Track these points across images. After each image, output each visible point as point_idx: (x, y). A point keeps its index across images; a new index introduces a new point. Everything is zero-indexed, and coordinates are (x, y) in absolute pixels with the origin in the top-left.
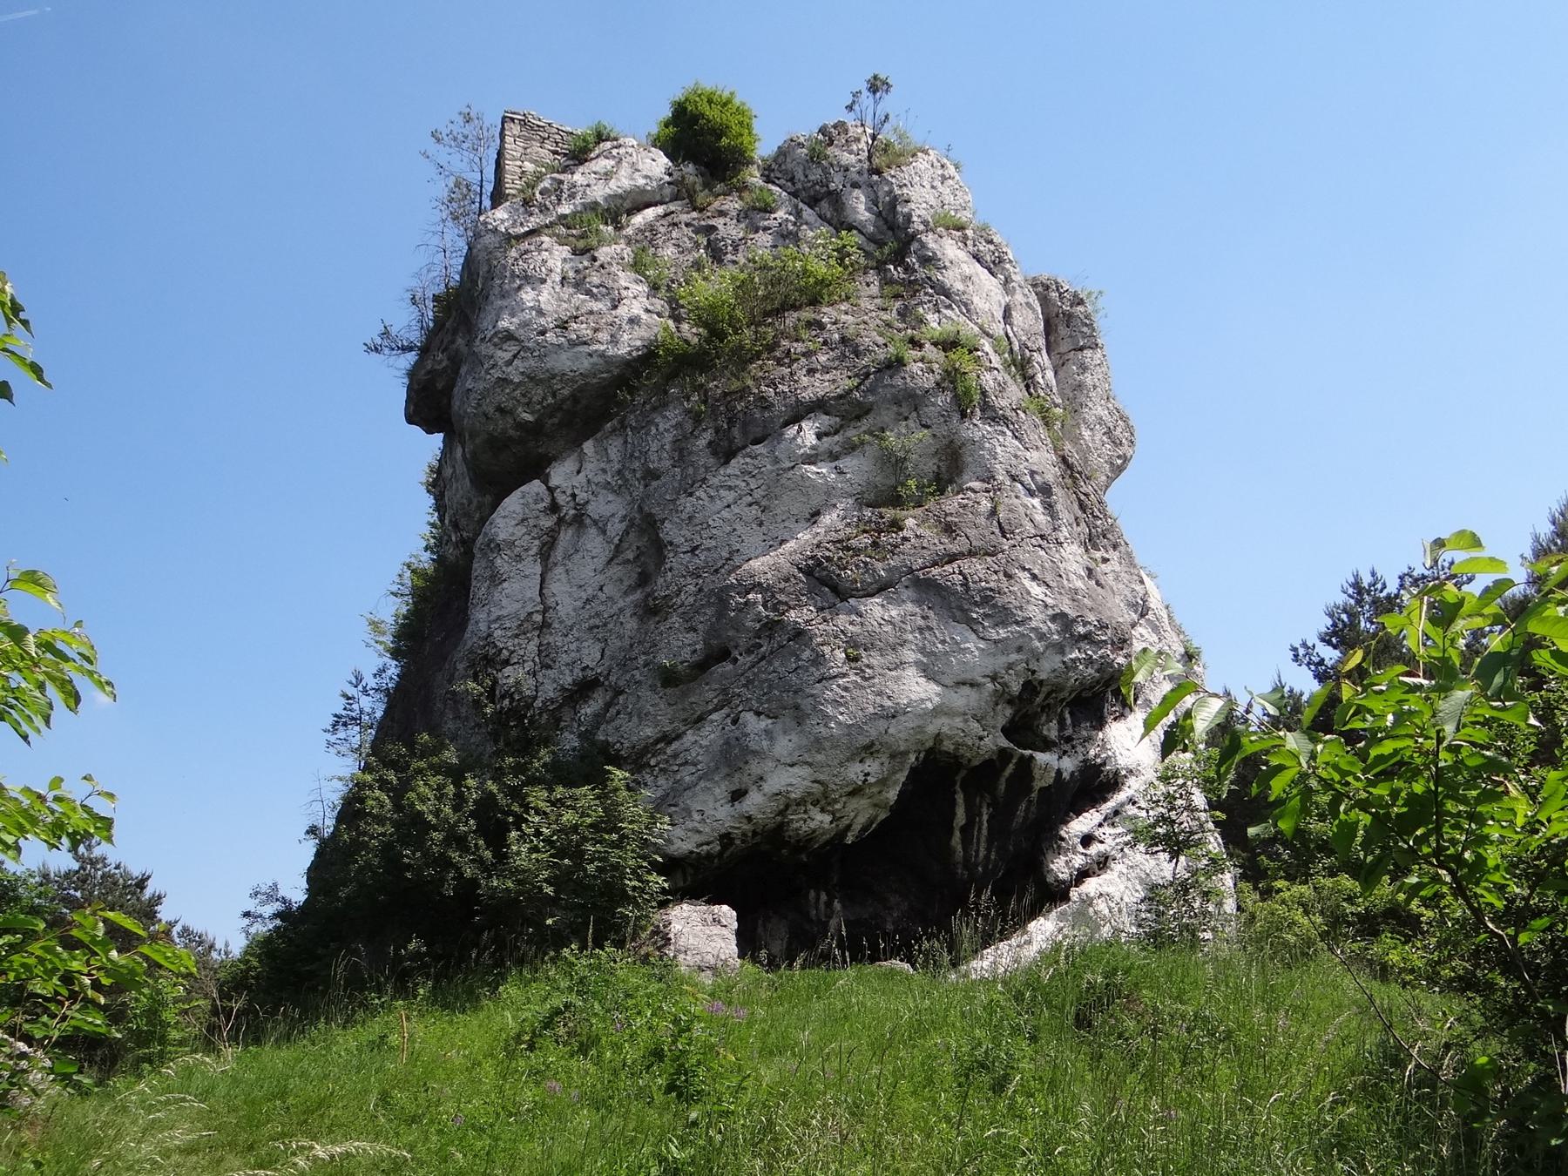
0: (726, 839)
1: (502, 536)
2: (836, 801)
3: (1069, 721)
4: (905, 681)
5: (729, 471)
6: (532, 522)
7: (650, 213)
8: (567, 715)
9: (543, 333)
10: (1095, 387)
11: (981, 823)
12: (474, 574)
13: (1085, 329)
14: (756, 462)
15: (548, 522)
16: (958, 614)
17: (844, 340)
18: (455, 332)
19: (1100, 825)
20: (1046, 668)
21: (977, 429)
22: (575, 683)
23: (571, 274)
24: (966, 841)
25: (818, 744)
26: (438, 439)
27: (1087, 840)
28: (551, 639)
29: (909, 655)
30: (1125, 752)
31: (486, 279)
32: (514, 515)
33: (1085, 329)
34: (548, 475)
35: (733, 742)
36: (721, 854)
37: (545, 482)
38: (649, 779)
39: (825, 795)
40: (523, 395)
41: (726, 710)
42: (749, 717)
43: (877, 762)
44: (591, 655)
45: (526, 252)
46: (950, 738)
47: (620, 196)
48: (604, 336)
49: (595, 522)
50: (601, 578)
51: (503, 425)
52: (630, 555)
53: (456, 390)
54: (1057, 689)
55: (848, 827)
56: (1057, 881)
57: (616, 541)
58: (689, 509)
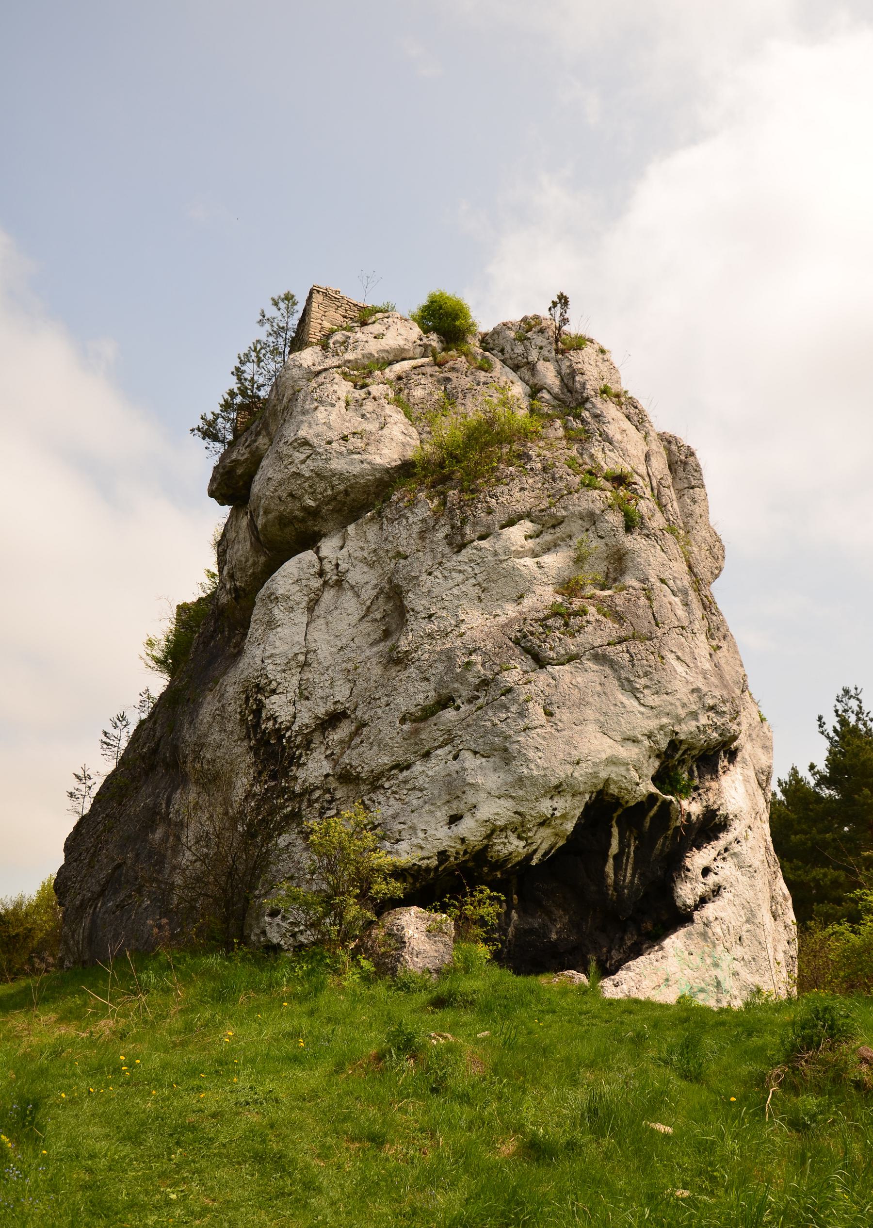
0: (443, 855)
1: (281, 591)
2: (530, 830)
3: (696, 774)
4: (588, 738)
5: (460, 558)
6: (304, 582)
7: (406, 365)
8: (317, 738)
9: (329, 443)
11: (629, 853)
12: (253, 618)
13: (695, 474)
14: (480, 553)
16: (626, 683)
18: (258, 434)
19: (715, 860)
20: (686, 729)
21: (634, 542)
22: (326, 714)
24: (617, 868)
25: (520, 781)
26: (227, 509)
27: (706, 871)
28: (310, 676)
29: (590, 713)
30: (732, 800)
31: (290, 400)
32: (292, 575)
33: (695, 474)
34: (318, 548)
35: (455, 775)
36: (437, 867)
37: (317, 552)
38: (382, 799)
39: (522, 825)
40: (310, 487)
41: (449, 748)
42: (467, 755)
43: (563, 799)
44: (341, 692)
45: (323, 384)
46: (615, 783)
47: (387, 351)
49: (352, 587)
50: (353, 631)
51: (293, 507)
52: (378, 616)
53: (257, 477)
54: (691, 747)
55: (535, 851)
56: (684, 905)
57: (368, 603)
58: (428, 585)
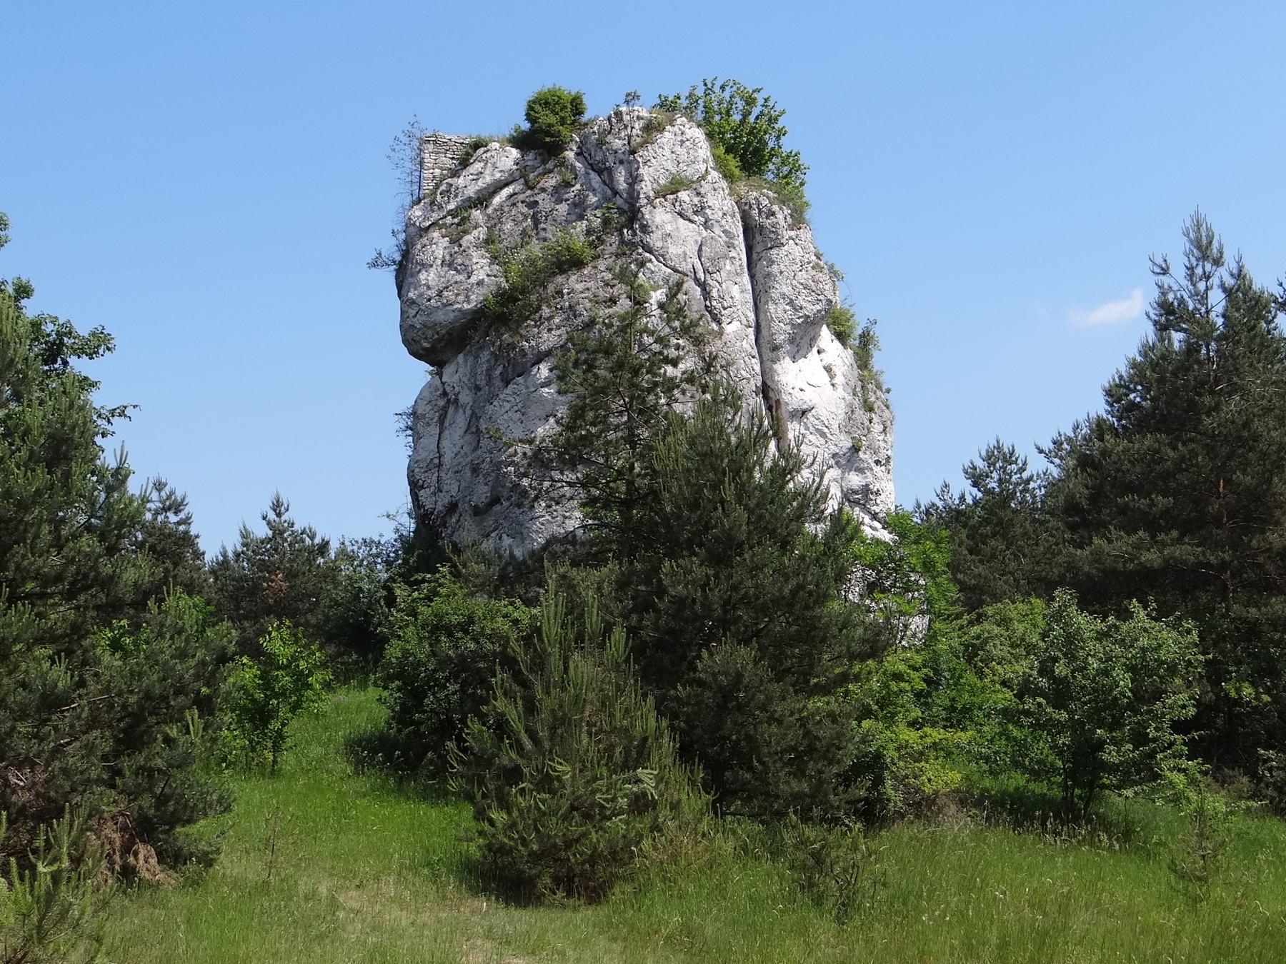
10: (781, 272)
15: (442, 403)
17: (570, 307)
23: (447, 258)
48: (461, 298)
